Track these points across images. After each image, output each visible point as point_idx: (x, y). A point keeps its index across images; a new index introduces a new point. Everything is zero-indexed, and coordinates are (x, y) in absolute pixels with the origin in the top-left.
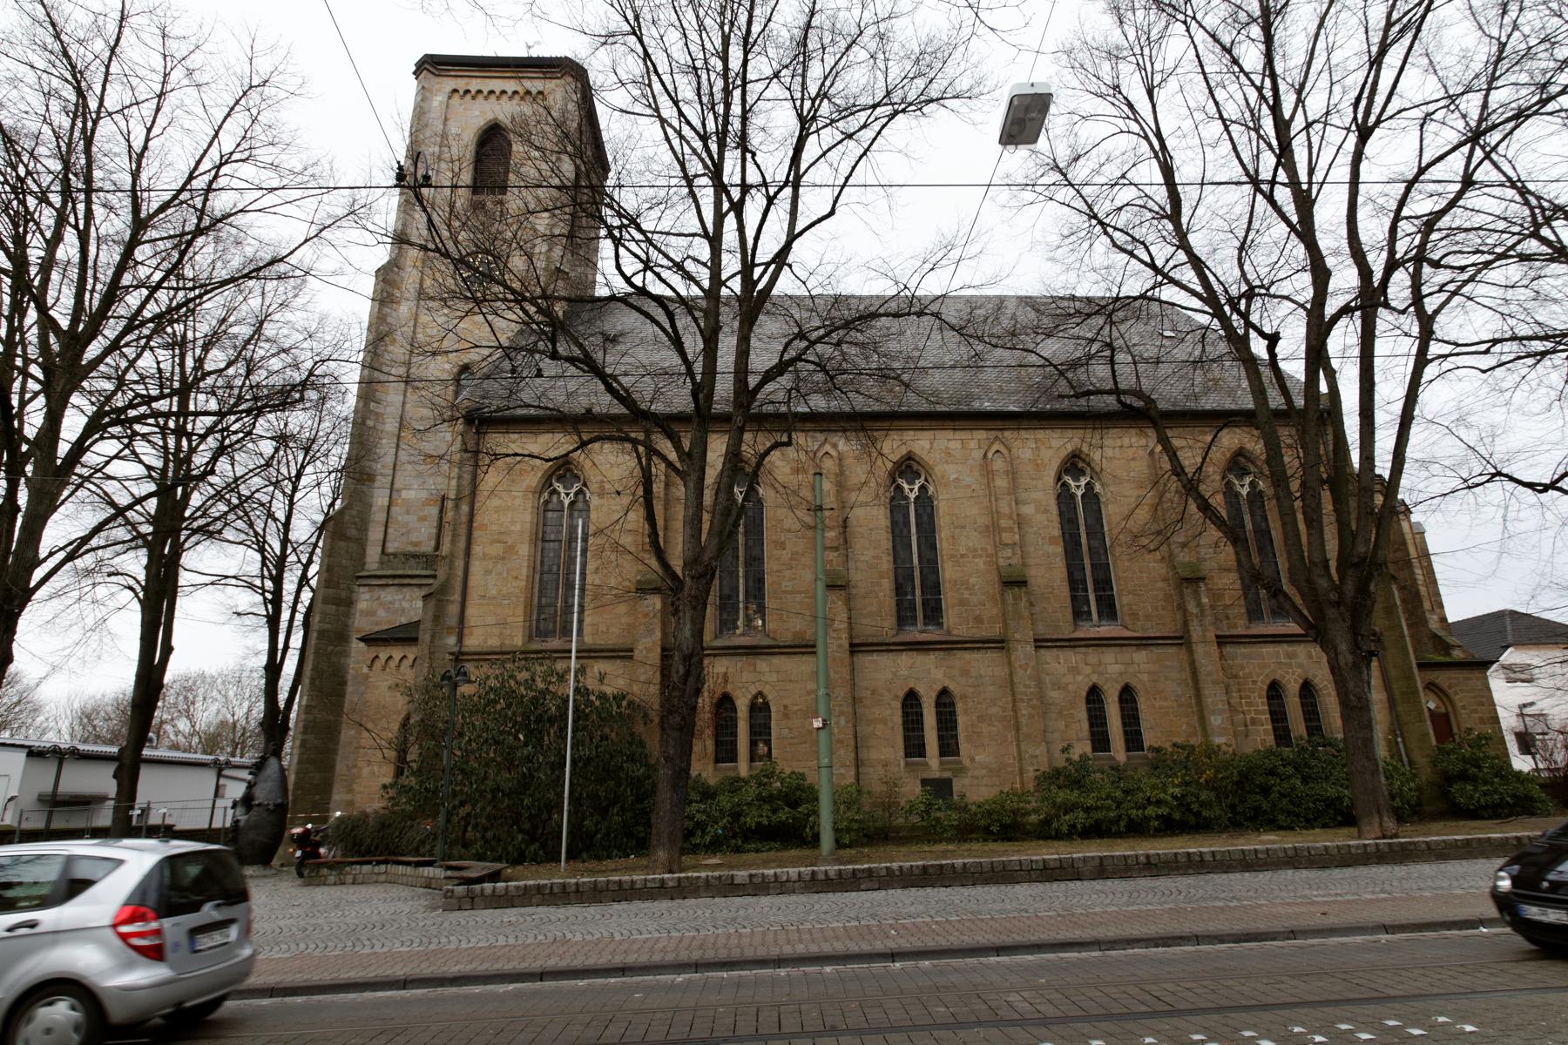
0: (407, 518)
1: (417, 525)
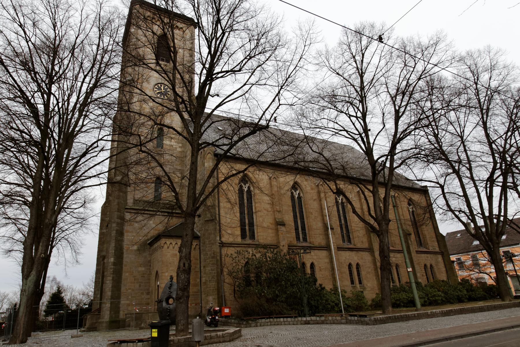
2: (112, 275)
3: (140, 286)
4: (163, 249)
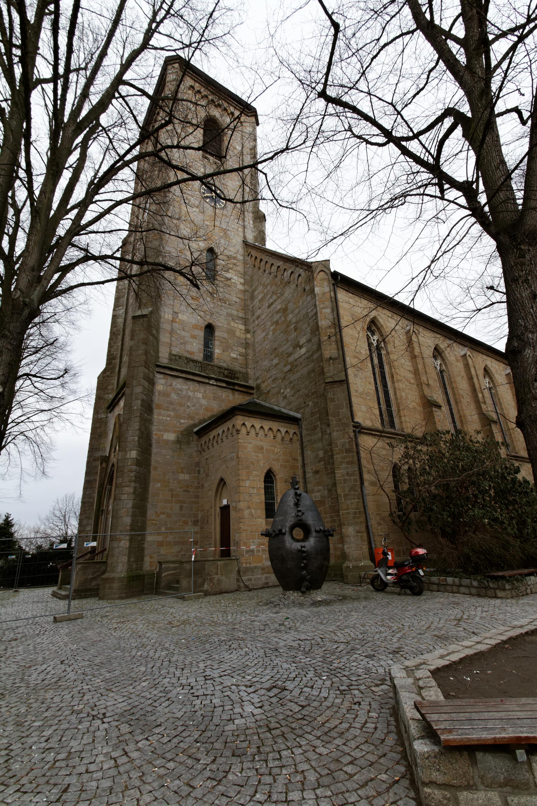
0: (183, 333)
1: (191, 340)
2: (133, 484)
3: (181, 508)
4: (240, 436)
